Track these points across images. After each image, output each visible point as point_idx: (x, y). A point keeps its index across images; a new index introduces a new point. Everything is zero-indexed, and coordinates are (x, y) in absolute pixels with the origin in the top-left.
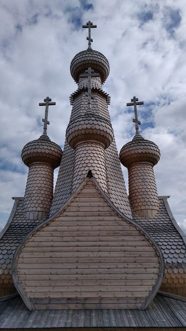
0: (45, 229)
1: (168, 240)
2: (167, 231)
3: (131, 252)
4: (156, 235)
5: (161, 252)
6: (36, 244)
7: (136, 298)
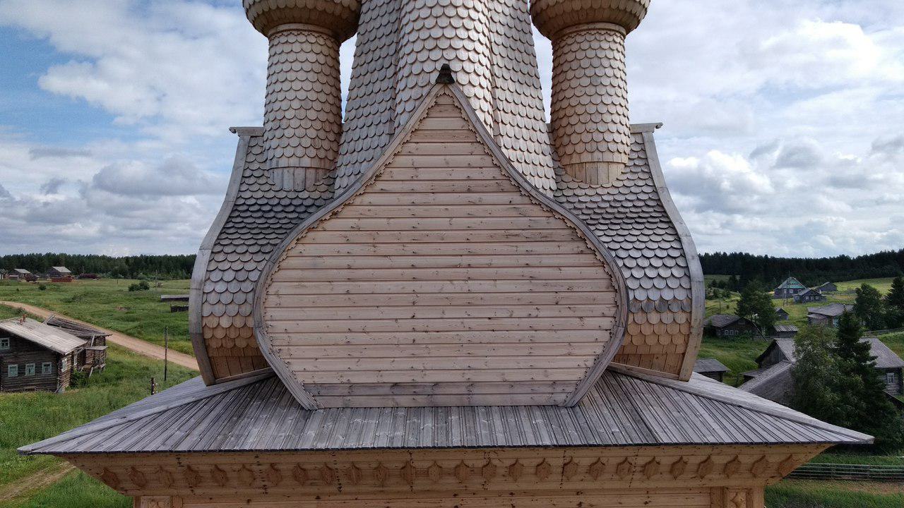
0: (328, 225)
1: (643, 246)
2: (644, 220)
3: (547, 282)
4: (615, 233)
5: (617, 265)
6: (308, 261)
7: (554, 382)
